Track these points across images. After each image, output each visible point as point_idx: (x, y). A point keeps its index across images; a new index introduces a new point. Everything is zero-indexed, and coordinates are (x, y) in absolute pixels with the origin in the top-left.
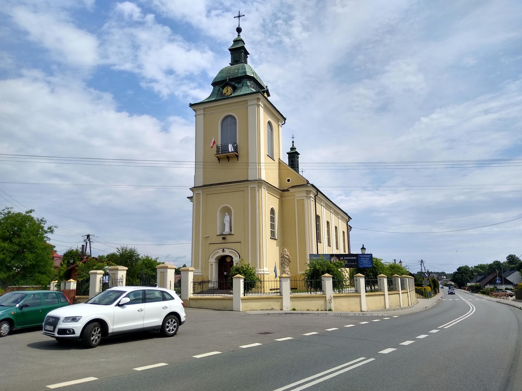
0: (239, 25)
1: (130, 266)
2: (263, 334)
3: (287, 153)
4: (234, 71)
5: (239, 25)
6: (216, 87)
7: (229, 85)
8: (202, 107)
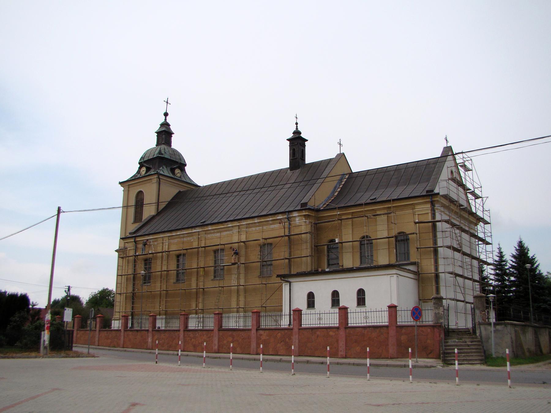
0: (166, 110)
2: (16, 404)
3: (287, 140)
5: (166, 110)
8: (127, 184)
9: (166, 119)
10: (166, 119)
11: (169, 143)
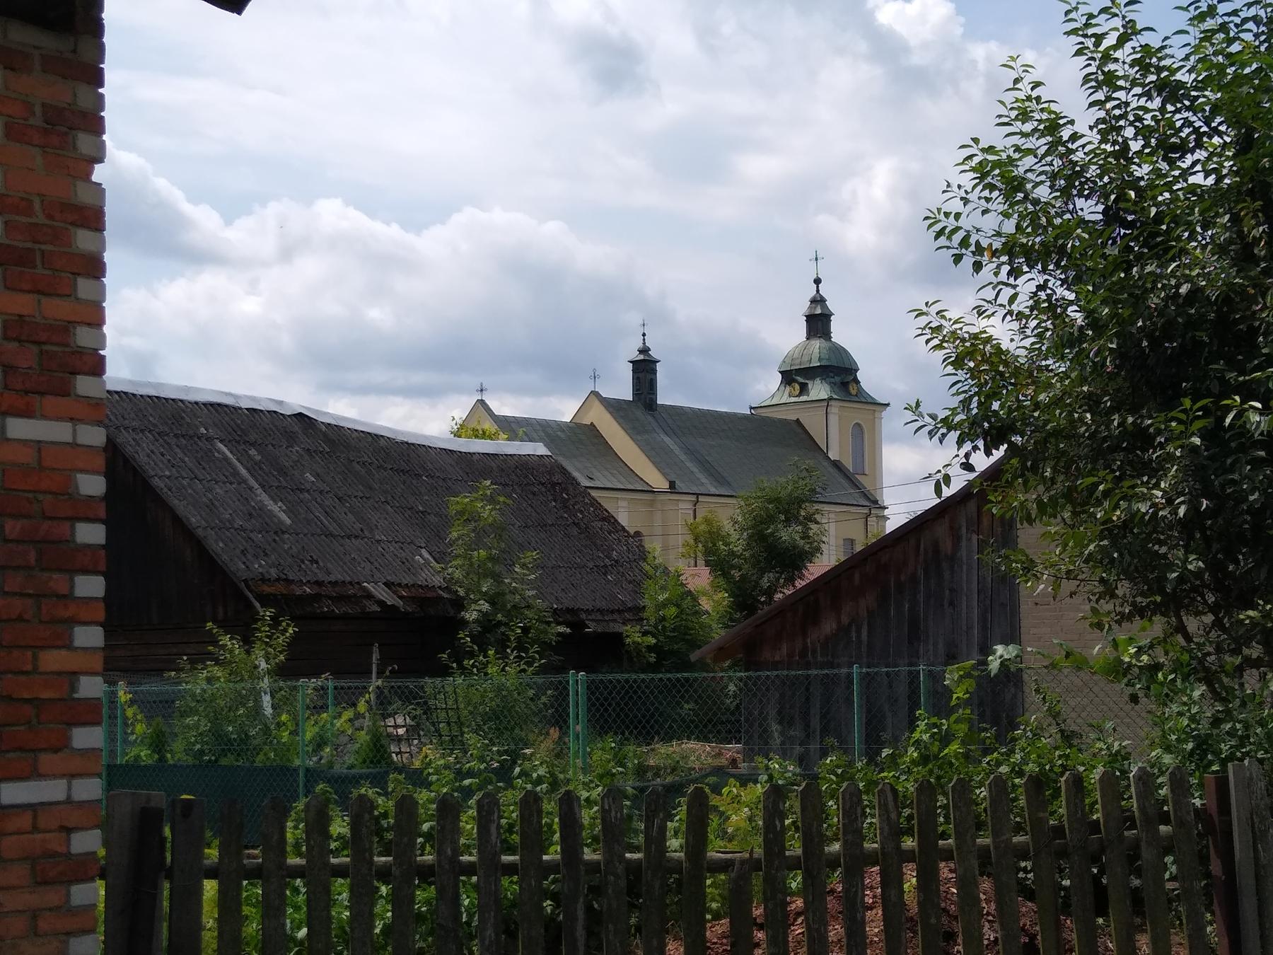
9: (818, 291)
10: (818, 291)
11: (826, 334)
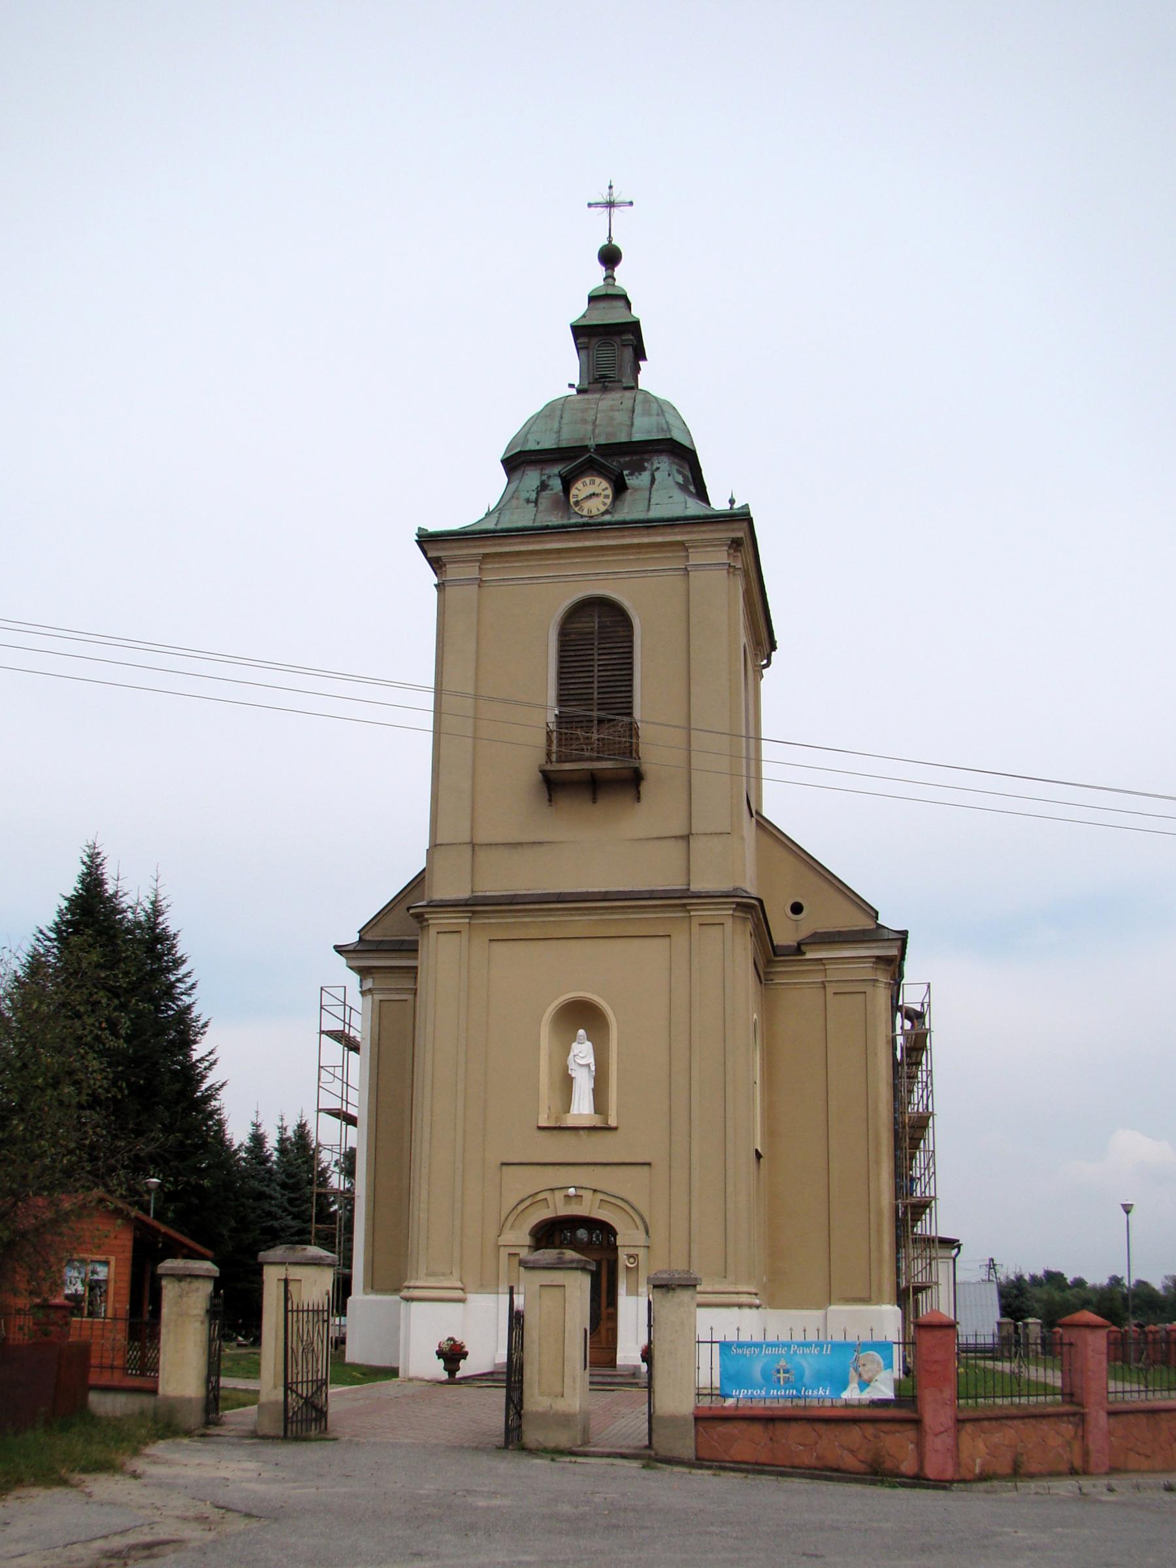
1: (86, 1312)
4: (611, 419)
6: (529, 473)
7: (596, 470)
